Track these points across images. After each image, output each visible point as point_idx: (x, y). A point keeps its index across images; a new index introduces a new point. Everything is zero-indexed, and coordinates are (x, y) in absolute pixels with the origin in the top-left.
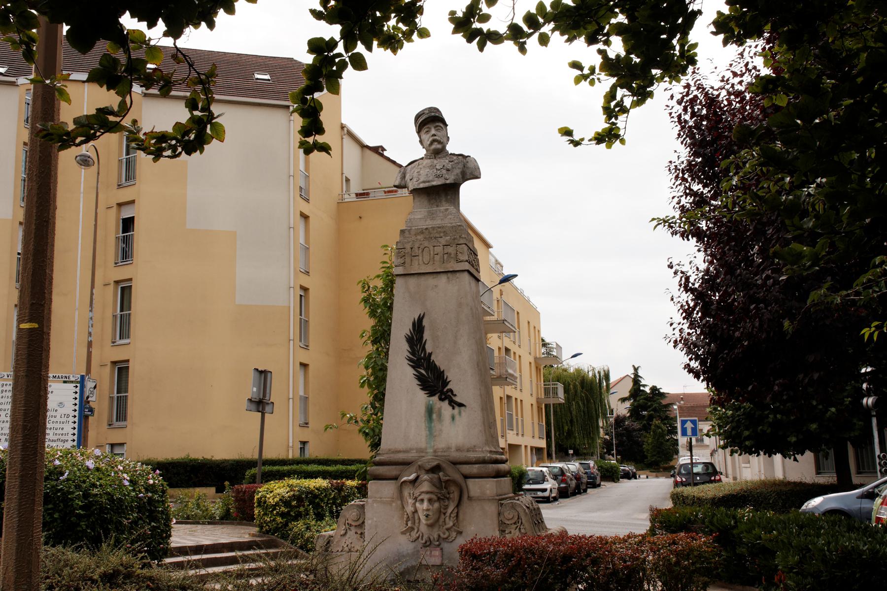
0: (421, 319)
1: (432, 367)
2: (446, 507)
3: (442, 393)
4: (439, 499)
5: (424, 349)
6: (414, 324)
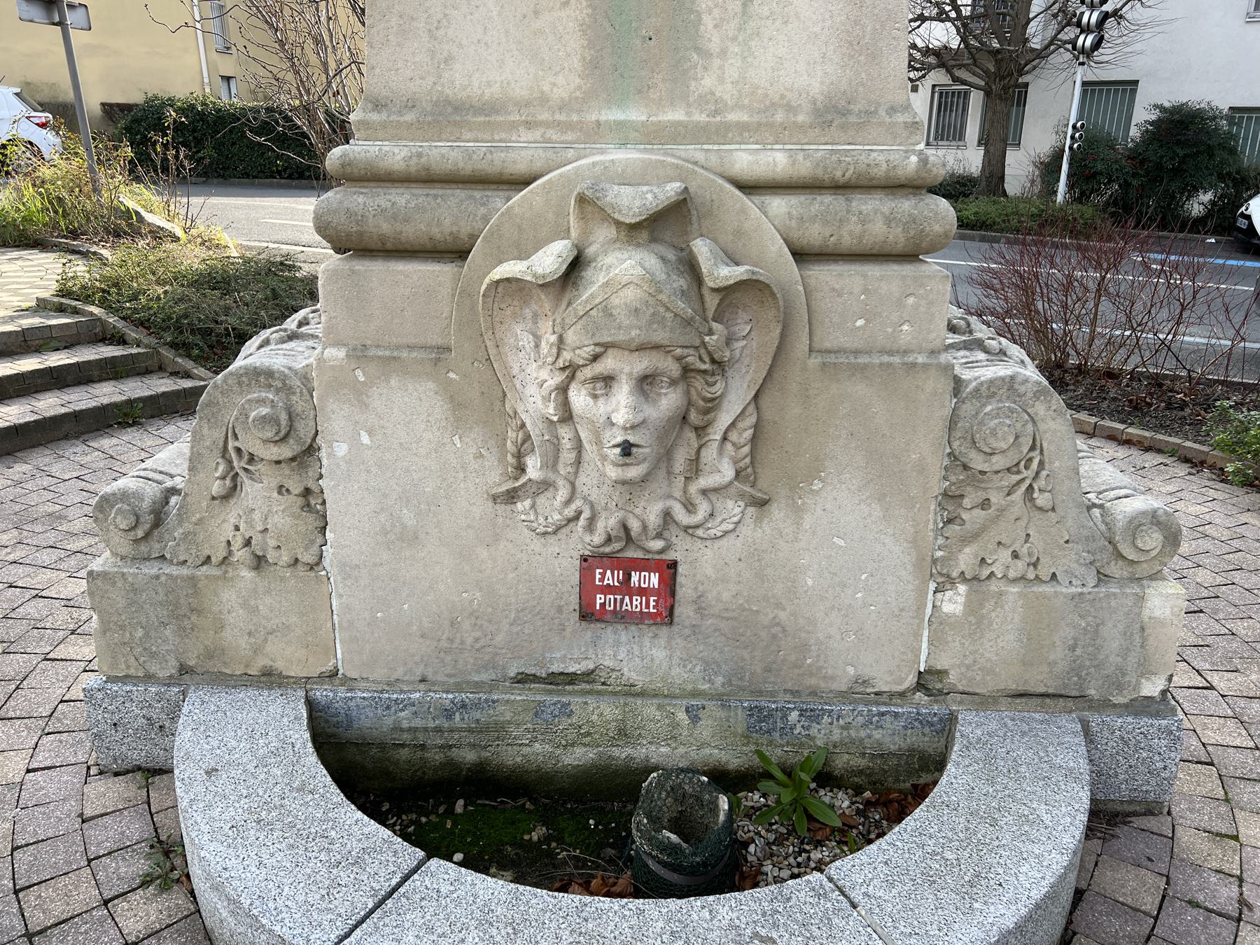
2: (712, 405)
4: (687, 371)
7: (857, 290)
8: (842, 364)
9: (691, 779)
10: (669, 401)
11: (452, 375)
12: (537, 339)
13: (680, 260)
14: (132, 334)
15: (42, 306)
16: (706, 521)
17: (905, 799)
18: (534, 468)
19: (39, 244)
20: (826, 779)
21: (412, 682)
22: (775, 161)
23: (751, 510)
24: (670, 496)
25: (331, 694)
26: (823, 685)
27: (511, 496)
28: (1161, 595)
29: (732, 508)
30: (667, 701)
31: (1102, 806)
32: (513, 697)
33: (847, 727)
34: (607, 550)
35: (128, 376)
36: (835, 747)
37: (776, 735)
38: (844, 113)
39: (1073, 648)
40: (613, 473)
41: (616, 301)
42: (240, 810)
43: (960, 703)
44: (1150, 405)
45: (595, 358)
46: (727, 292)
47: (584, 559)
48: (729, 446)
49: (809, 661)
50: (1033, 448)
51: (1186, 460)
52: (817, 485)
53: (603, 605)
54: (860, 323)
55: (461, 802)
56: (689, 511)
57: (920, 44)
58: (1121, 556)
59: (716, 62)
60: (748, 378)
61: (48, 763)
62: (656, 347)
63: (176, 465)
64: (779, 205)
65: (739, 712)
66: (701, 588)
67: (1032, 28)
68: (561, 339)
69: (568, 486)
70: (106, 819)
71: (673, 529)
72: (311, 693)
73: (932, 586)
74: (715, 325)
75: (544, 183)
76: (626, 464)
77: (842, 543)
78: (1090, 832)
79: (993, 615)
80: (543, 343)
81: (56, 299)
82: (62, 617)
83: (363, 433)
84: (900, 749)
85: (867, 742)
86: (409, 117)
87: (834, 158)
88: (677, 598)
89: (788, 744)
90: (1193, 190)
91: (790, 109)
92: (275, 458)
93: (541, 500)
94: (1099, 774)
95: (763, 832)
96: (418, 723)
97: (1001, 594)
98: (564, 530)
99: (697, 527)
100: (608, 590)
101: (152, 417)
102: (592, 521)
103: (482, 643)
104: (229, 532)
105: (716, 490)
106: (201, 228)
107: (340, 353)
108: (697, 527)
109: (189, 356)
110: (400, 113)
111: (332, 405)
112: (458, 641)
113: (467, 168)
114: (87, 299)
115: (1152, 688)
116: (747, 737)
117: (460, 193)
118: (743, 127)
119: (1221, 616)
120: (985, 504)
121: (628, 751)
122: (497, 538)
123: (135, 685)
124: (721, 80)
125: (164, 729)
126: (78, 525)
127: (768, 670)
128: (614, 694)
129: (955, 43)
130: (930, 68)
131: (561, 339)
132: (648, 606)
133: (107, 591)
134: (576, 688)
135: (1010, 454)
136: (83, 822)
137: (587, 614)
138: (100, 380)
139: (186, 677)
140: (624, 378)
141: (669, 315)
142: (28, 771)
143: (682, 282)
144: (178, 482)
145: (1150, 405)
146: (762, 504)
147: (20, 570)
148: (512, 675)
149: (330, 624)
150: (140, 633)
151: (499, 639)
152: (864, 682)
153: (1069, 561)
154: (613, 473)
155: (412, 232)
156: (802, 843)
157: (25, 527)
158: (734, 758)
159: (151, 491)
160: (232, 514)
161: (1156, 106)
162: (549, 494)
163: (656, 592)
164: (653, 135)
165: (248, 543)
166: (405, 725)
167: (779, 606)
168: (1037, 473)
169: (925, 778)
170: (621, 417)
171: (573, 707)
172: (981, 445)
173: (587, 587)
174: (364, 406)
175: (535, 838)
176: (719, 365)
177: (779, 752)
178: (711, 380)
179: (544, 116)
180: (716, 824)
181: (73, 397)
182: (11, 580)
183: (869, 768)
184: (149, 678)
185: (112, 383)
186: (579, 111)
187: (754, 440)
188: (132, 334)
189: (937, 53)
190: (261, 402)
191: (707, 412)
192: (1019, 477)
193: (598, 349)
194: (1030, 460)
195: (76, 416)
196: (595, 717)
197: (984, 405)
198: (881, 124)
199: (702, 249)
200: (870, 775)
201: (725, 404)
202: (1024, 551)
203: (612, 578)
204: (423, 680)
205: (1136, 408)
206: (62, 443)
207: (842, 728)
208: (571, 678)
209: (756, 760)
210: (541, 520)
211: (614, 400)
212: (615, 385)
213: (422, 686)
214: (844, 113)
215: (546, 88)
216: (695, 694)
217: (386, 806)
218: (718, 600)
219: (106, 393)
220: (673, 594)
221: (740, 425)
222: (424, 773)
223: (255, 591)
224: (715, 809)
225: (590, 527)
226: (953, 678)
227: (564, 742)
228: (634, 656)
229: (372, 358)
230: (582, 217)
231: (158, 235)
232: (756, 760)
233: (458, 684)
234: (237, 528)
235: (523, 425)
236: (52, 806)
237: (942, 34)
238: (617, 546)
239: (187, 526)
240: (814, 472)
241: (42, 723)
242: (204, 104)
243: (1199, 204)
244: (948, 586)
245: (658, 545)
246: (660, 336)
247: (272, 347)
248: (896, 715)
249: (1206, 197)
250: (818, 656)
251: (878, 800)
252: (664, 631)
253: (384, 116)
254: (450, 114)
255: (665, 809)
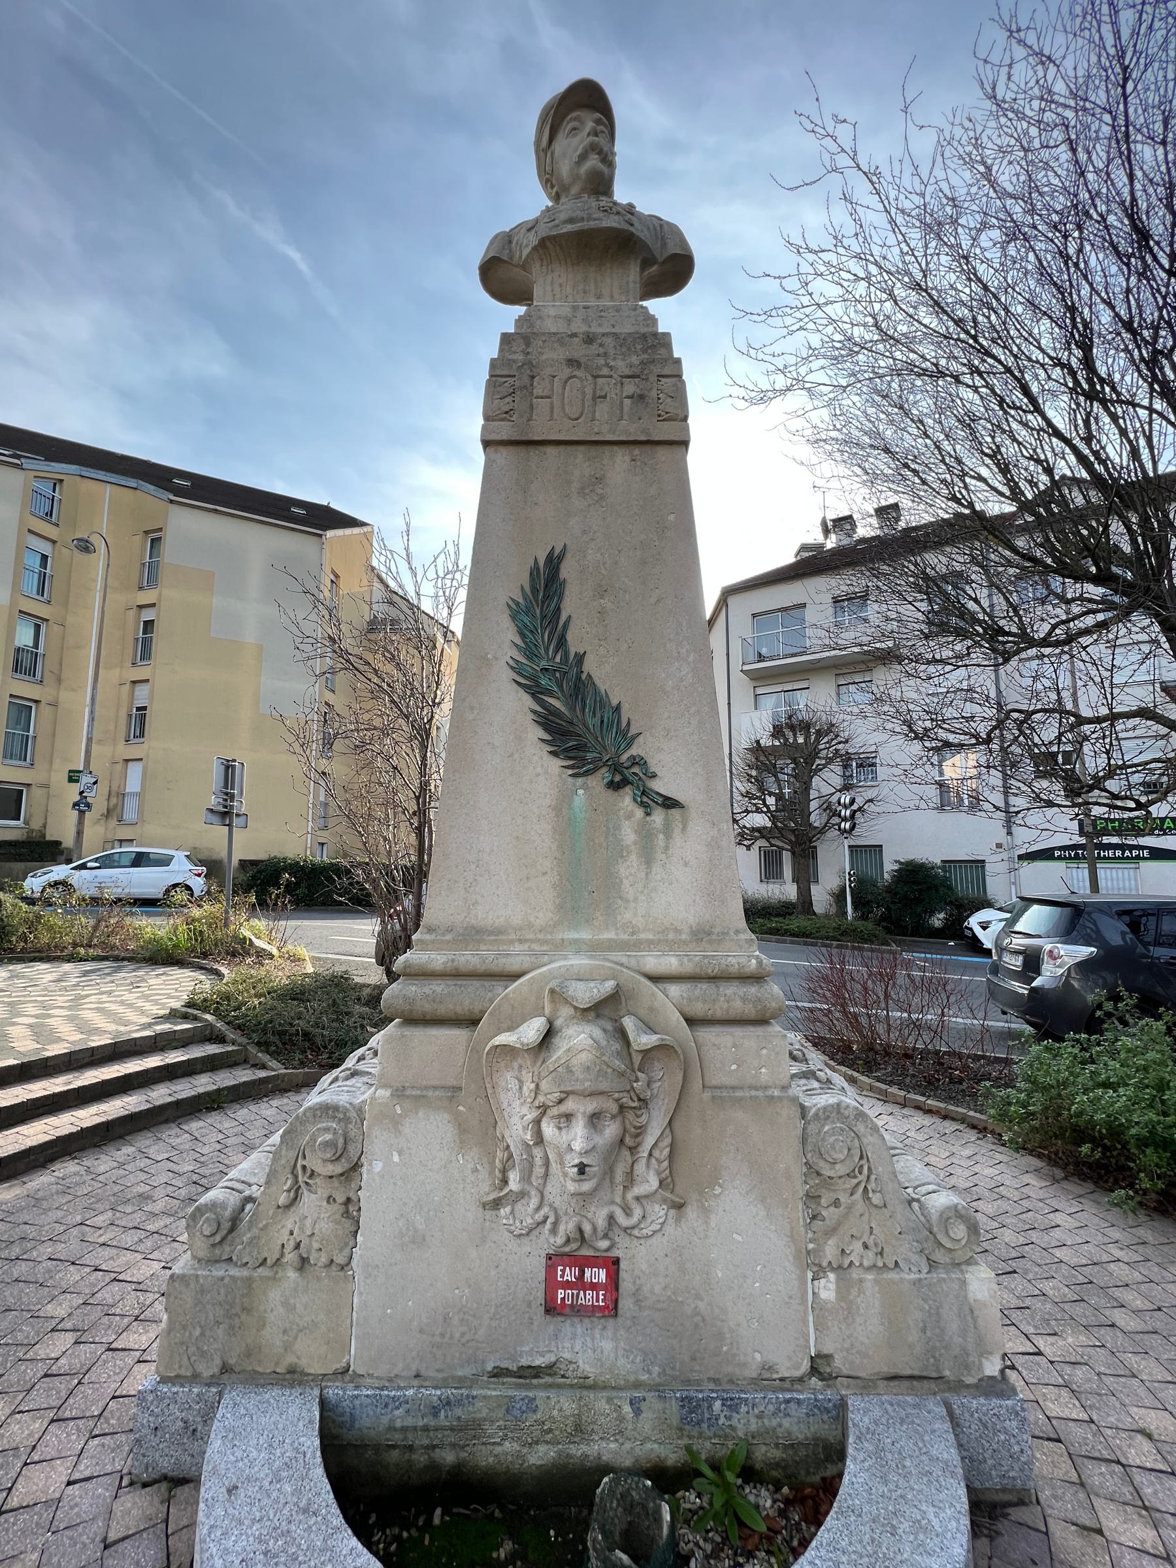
0: (554, 562)
1: (580, 688)
2: (640, 1131)
3: (616, 768)
4: (622, 1108)
5: (562, 643)
6: (534, 572)
7: (729, 1045)
8: (726, 1096)
9: (637, 1483)
10: (611, 1130)
11: (461, 1108)
12: (521, 1082)
13: (615, 1029)
14: (231, 1036)
15: (174, 1015)
16: (640, 1222)
17: (818, 1495)
18: (514, 1182)
19: (180, 963)
20: (750, 1474)
21: (409, 1378)
22: (670, 963)
23: (672, 1212)
24: (613, 1202)
25: (341, 1392)
26: (738, 1372)
27: (496, 1204)
28: (978, 1279)
29: (658, 1211)
30: (614, 1394)
31: (982, 1497)
32: (489, 1393)
33: (760, 1416)
34: (567, 1249)
35: (221, 1068)
36: (753, 1438)
37: (705, 1426)
38: (709, 934)
39: (924, 1330)
40: (571, 1187)
41: (574, 1061)
42: (251, 1539)
43: (848, 1387)
44: (939, 1080)
45: (560, 1101)
46: (646, 1053)
47: (549, 1257)
48: (653, 1161)
49: (725, 1348)
50: (861, 1158)
51: (974, 1127)
52: (718, 1190)
53: (563, 1299)
54: (734, 1067)
55: (438, 1511)
56: (627, 1214)
57: (748, 826)
58: (940, 1245)
59: (632, 905)
60: (663, 1109)
61: (87, 1474)
62: (602, 1093)
63: (255, 1174)
64: (675, 990)
65: (673, 1403)
66: (638, 1282)
67: (813, 818)
68: (537, 1086)
69: (539, 1195)
70: (126, 1544)
71: (616, 1230)
72: (325, 1391)
73: (810, 1275)
74: (639, 1074)
75: (529, 980)
76: (581, 1180)
77: (740, 1239)
78: (976, 1530)
79: (859, 1300)
80: (525, 1088)
81: (184, 1009)
82: (131, 1303)
83: (395, 1153)
84: (807, 1439)
85: (780, 1431)
86: (448, 937)
87: (706, 961)
88: (620, 1291)
89: (715, 1436)
90: (932, 913)
91: (677, 931)
92: (329, 1174)
93: (519, 1206)
94: (972, 1460)
95: (701, 1542)
96: (409, 1422)
97: (861, 1281)
98: (534, 1232)
99: (633, 1228)
100: (567, 1285)
101: (232, 1101)
102: (555, 1224)
103: (467, 1337)
104: (284, 1236)
105: (646, 1197)
106: (290, 947)
107: (384, 1094)
108: (633, 1228)
109: (267, 1052)
110: (443, 935)
111: (376, 1131)
112: (448, 1336)
113: (481, 968)
114: (206, 1010)
115: (992, 1368)
116: (681, 1429)
117: (476, 983)
118: (650, 942)
119: (1030, 1276)
120: (836, 1203)
121: (583, 1448)
122: (484, 1239)
123: (182, 1386)
124: (635, 915)
125: (195, 1433)
126: (158, 1207)
127: (693, 1359)
128: (572, 1386)
129: (769, 824)
130: (756, 839)
131: (537, 1086)
132: (598, 1301)
133: (180, 1293)
134: (541, 1381)
135: (847, 1162)
136: (106, 1548)
137: (551, 1309)
138: (201, 1072)
139: (225, 1376)
140: (580, 1116)
141: (609, 1070)
142: (69, 1483)
143: (617, 1046)
144: (255, 1191)
145: (939, 1080)
146: (679, 1207)
147: (108, 1252)
148: (490, 1369)
149: (349, 1321)
150: (197, 1332)
151: (482, 1332)
152: (770, 1367)
153: (904, 1250)
154: (571, 1187)
155: (442, 1010)
156: (736, 1554)
157: (119, 1208)
158: (672, 1455)
159: (234, 1199)
160: (290, 1221)
161: (896, 862)
162: (523, 1202)
163: (604, 1287)
164: (595, 947)
165: (298, 1246)
166: (398, 1424)
167: (698, 1297)
168: (868, 1177)
169: (831, 1471)
170: (577, 1146)
171: (538, 1402)
172: (826, 1156)
173: (551, 1284)
174: (398, 1132)
175: (503, 1556)
176: (644, 1102)
177: (708, 1445)
178: (639, 1113)
179: (531, 936)
180: (661, 1537)
181: (179, 1087)
182: (98, 1262)
183: (783, 1460)
184: (195, 1378)
185: (209, 1074)
186: (551, 933)
187: (671, 1156)
188: (231, 1036)
189: (759, 830)
190: (327, 1130)
191: (637, 1135)
192: (855, 1181)
193: (563, 1096)
194: (861, 1166)
195: (178, 1104)
196: (555, 1412)
197: (823, 1126)
198: (732, 940)
199: (629, 1023)
200: (785, 1468)
201: (649, 1130)
202: (871, 1242)
203: (570, 1275)
204: (417, 1376)
205: (930, 1083)
206: (162, 1126)
207: (757, 1417)
208: (536, 1372)
209: (687, 1458)
210: (518, 1223)
211: (573, 1131)
212: (574, 1121)
213: (416, 1383)
214: (709, 934)
215: (532, 919)
216: (637, 1385)
217: (373, 1518)
218: (652, 1292)
219: (204, 1083)
220: (617, 1289)
221: (661, 1145)
222: (409, 1477)
223: (295, 1290)
224: (658, 1519)
225: (554, 1231)
226: (838, 1362)
227: (530, 1440)
228: (589, 1349)
229: (408, 1097)
230: (553, 1001)
231: (261, 954)
232: (687, 1458)
233: (445, 1379)
234: (292, 1233)
235: (508, 1146)
236: (80, 1529)
237: (760, 820)
238: (574, 1246)
239: (255, 1231)
240: (714, 1179)
241: (91, 1423)
242: (305, 861)
243: (938, 920)
244: (821, 1275)
245: (604, 1244)
246: (604, 1086)
247: (340, 1083)
248: (799, 1402)
249: (942, 916)
250: (732, 1344)
251: (795, 1497)
252: (611, 1323)
253: (433, 937)
254: (473, 935)
255: (616, 1520)
